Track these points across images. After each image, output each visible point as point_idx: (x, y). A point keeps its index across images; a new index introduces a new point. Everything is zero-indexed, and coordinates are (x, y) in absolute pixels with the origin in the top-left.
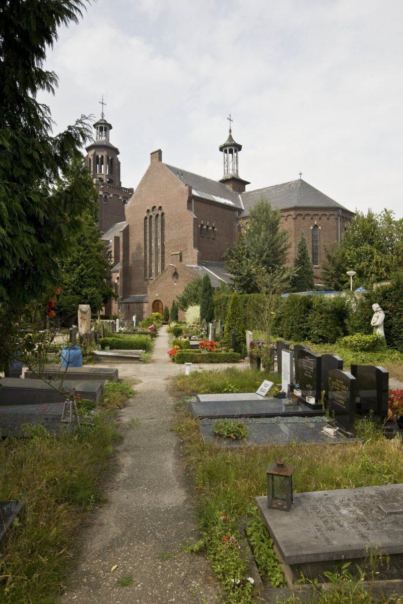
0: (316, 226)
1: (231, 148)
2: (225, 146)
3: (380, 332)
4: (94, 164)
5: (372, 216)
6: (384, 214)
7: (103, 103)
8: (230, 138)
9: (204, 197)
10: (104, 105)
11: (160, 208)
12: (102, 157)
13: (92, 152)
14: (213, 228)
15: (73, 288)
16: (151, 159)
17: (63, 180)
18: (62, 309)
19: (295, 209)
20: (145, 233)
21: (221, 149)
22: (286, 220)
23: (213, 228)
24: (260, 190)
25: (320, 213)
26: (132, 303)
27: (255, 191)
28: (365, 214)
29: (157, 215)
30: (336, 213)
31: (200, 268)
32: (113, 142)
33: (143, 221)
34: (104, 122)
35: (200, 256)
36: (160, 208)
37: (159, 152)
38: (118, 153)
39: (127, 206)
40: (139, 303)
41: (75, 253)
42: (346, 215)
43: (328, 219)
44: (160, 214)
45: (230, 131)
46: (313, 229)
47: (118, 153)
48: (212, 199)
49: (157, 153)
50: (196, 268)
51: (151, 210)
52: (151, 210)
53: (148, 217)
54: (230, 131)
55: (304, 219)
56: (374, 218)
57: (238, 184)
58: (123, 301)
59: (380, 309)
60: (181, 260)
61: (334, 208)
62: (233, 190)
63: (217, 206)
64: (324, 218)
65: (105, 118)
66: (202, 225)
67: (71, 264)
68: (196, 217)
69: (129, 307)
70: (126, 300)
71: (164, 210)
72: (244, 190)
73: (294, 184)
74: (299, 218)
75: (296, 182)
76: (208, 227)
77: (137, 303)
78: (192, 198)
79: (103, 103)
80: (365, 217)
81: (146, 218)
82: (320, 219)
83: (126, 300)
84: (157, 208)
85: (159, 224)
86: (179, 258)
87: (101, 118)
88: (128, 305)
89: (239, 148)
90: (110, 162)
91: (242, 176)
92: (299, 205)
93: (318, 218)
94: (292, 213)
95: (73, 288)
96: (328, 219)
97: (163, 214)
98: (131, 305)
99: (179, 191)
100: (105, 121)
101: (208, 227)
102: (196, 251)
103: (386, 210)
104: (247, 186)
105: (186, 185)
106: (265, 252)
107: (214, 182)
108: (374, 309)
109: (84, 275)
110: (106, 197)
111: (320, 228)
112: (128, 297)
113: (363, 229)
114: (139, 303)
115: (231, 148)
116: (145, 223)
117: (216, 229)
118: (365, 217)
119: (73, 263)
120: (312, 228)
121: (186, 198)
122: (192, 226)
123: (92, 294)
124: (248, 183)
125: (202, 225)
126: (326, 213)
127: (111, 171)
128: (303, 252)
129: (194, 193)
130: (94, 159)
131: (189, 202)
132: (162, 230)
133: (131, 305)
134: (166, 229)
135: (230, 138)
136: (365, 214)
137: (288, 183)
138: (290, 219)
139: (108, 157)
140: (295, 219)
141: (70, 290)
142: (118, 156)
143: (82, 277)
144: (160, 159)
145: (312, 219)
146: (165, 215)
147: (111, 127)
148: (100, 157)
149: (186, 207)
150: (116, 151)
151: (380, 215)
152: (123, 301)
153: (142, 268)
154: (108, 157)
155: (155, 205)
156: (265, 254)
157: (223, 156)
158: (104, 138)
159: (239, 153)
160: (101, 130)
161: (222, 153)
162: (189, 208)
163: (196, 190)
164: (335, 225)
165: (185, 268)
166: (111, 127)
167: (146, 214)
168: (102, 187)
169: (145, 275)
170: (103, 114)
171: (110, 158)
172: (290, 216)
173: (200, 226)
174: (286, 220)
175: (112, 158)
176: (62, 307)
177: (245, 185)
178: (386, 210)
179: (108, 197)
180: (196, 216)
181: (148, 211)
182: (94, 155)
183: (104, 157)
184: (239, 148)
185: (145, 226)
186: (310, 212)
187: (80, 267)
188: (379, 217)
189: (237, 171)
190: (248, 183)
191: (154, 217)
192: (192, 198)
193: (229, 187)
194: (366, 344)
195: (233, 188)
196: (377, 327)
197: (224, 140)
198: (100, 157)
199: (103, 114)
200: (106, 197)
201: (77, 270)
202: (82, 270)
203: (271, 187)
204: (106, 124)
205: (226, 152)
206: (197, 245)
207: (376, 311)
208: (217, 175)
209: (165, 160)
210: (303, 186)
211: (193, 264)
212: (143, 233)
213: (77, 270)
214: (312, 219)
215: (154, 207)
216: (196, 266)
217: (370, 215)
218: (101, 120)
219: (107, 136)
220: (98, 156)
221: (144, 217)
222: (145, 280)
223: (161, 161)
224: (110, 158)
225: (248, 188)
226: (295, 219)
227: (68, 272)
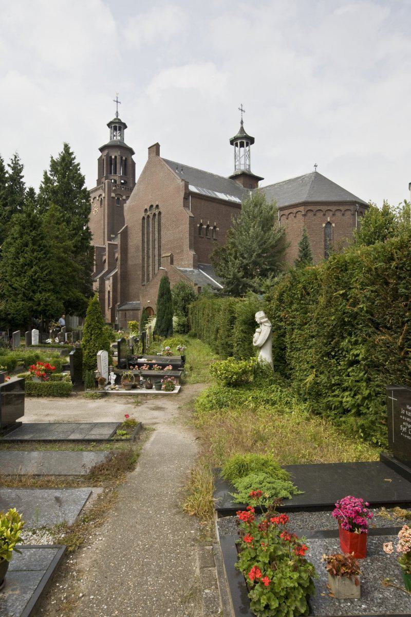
0: (329, 223)
1: (243, 140)
2: (236, 139)
3: (265, 356)
4: (107, 165)
5: (388, 209)
6: (403, 207)
7: (117, 102)
8: (242, 130)
9: (204, 193)
10: (119, 103)
11: (157, 206)
12: (116, 157)
13: (106, 152)
14: (215, 227)
15: (24, 293)
16: (149, 154)
17: (52, 178)
18: (9, 317)
19: (305, 204)
20: (143, 234)
21: (232, 142)
22: (295, 217)
23: (215, 227)
24: (272, 185)
25: (334, 208)
26: (128, 310)
27: (267, 187)
28: (380, 206)
29: (155, 215)
30: (352, 208)
31: (196, 271)
32: (128, 142)
33: (141, 221)
34: (117, 121)
35: (196, 258)
36: (157, 206)
37: (157, 146)
38: (133, 153)
39: (127, 206)
40: (134, 310)
41: (29, 253)
42: (362, 207)
43: (343, 215)
44: (157, 213)
45: (242, 123)
46: (326, 227)
47: (133, 153)
48: (214, 196)
49: (155, 147)
50: (190, 271)
51: (148, 209)
52: (148, 209)
53: (146, 217)
54: (242, 123)
55: (315, 215)
56: (390, 210)
57: (248, 179)
58: (121, 308)
59: (266, 319)
60: (172, 262)
61: (350, 202)
62: (244, 187)
63: (220, 203)
64: (339, 214)
65: (119, 117)
66: (201, 225)
67: (23, 266)
68: (192, 215)
69: (125, 315)
70: (123, 307)
71: (161, 209)
72: (257, 186)
73: (308, 177)
74: (310, 214)
75: (310, 176)
76: (208, 226)
77: (133, 310)
78: (188, 195)
79: (117, 102)
80: (381, 210)
81: (144, 218)
82: (334, 215)
83: (123, 307)
84: (154, 207)
85: (156, 223)
86: (169, 261)
87: (115, 117)
88: (124, 312)
89: (251, 140)
90: (124, 163)
91: (255, 172)
92: (310, 200)
93: (331, 213)
94: (302, 209)
95: (24, 293)
96: (343, 215)
97: (160, 213)
98: (127, 312)
99: (176, 187)
100: (119, 120)
101: (208, 226)
102: (192, 253)
103: (405, 202)
104: (260, 182)
105: (183, 180)
106: (254, 251)
107: (223, 178)
108: (257, 320)
109: (38, 278)
110: (118, 199)
111: (333, 225)
112: (126, 304)
113: (376, 223)
114: (134, 310)
115: (243, 140)
116: (143, 223)
117: (218, 229)
118: (381, 210)
119: (26, 265)
120: (324, 225)
121: (182, 194)
122: (188, 226)
123: (46, 300)
124: (261, 179)
125: (201, 225)
126: (341, 208)
127: (125, 173)
128: (304, 252)
129: (192, 188)
130: (107, 160)
131: (186, 198)
132: (159, 231)
133: (127, 312)
134: (162, 229)
135: (242, 130)
136: (380, 206)
137: (302, 176)
138: (299, 216)
139: (122, 158)
140: (305, 215)
141: (20, 296)
142: (133, 157)
143: (35, 281)
144: (158, 153)
145: (324, 215)
146: (162, 215)
147: (125, 127)
148: (113, 157)
149: (182, 204)
150: (132, 152)
151: (398, 208)
152: (121, 308)
153: (140, 273)
154: (122, 158)
155: (152, 203)
156: (255, 254)
157: (234, 149)
158: (119, 138)
159: (252, 146)
160: (115, 129)
161: (233, 147)
162: (186, 205)
163: (196, 186)
164: (351, 221)
165: (176, 271)
166: (125, 127)
167: (143, 214)
168: (114, 188)
169: (143, 280)
170: (117, 112)
171: (124, 158)
172: (299, 213)
173: (198, 225)
174: (295, 217)
175: (126, 159)
176: (9, 314)
177: (258, 182)
178: (405, 202)
179: (121, 199)
180: (193, 214)
181: (146, 210)
182: (107, 155)
183: (118, 157)
184: (251, 140)
185: (143, 227)
186: (321, 207)
187: (33, 270)
188: (397, 210)
189: (249, 165)
190: (261, 179)
191: (151, 216)
192: (188, 195)
193: (239, 183)
194: (232, 376)
195: (243, 184)
196: (260, 348)
197: (235, 133)
198: (113, 157)
199: (117, 112)
200: (118, 199)
201: (30, 273)
202: (35, 272)
203: (283, 182)
204: (120, 122)
205: (237, 145)
206: (194, 245)
207: (261, 323)
208: (226, 170)
209: (164, 154)
210: (318, 179)
211: (189, 267)
212: (140, 234)
213: (30, 273)
214: (324, 215)
215: (152, 206)
216: (192, 269)
217: (386, 207)
218: (115, 119)
219: (122, 135)
220: (111, 157)
221: (141, 218)
222: (143, 285)
223: (159, 155)
224: (124, 158)
225: (261, 184)
226: (305, 215)
227: (19, 275)
